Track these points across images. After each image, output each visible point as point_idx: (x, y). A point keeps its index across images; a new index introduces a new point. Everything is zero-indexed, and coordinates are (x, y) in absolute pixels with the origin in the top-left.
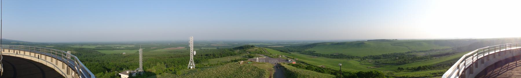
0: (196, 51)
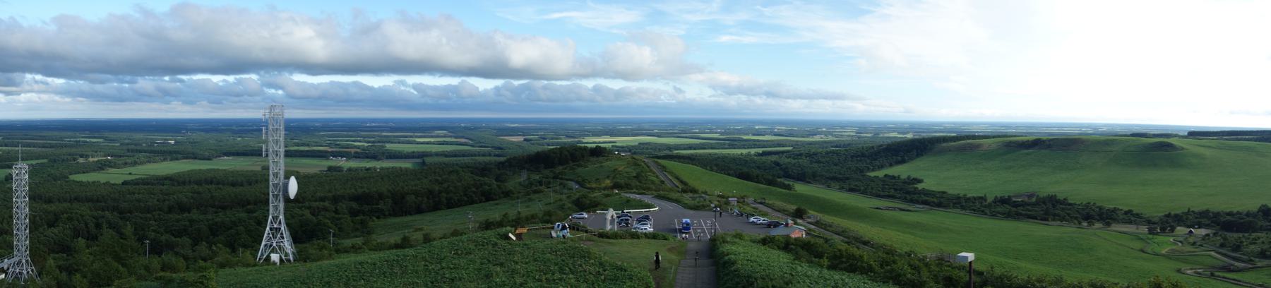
0: (297, 178)
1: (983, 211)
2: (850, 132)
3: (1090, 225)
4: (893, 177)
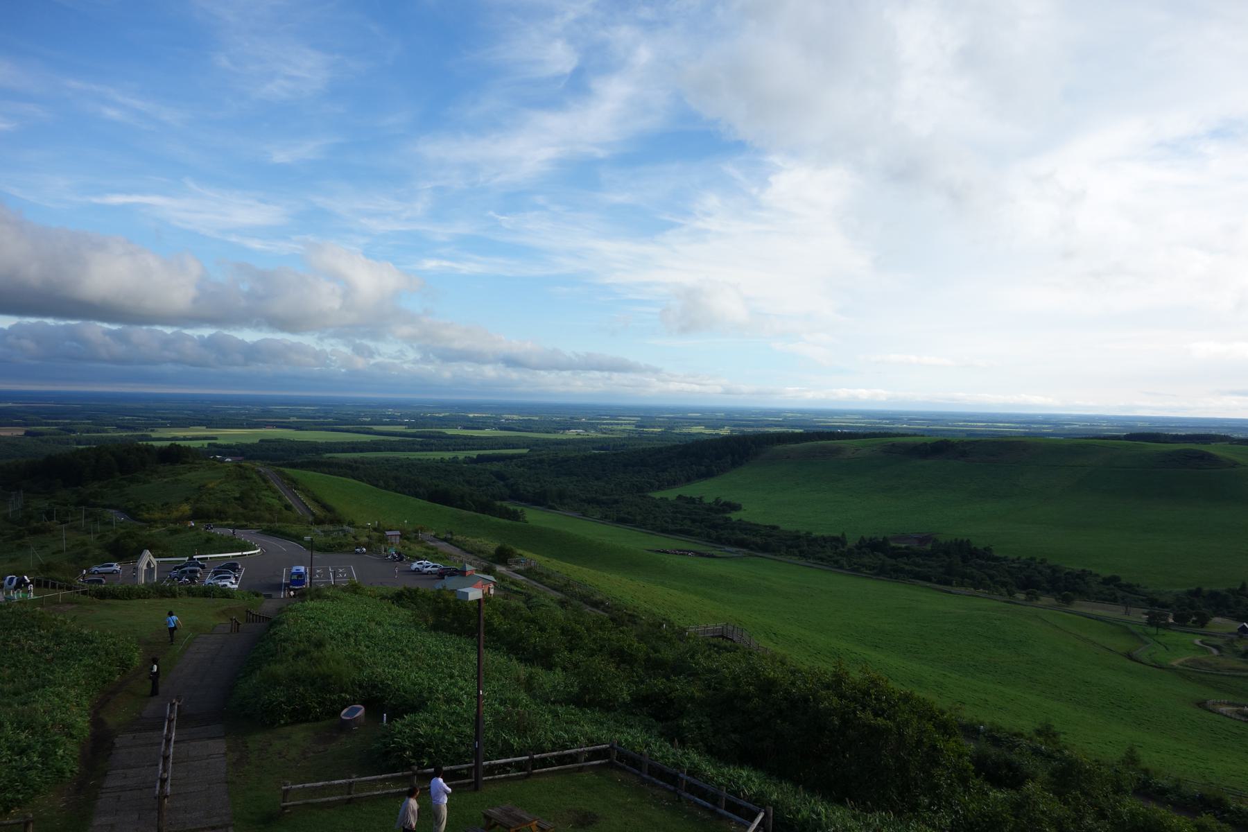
1: (836, 562)
2: (626, 426)
3: (1031, 600)
4: (691, 501)
